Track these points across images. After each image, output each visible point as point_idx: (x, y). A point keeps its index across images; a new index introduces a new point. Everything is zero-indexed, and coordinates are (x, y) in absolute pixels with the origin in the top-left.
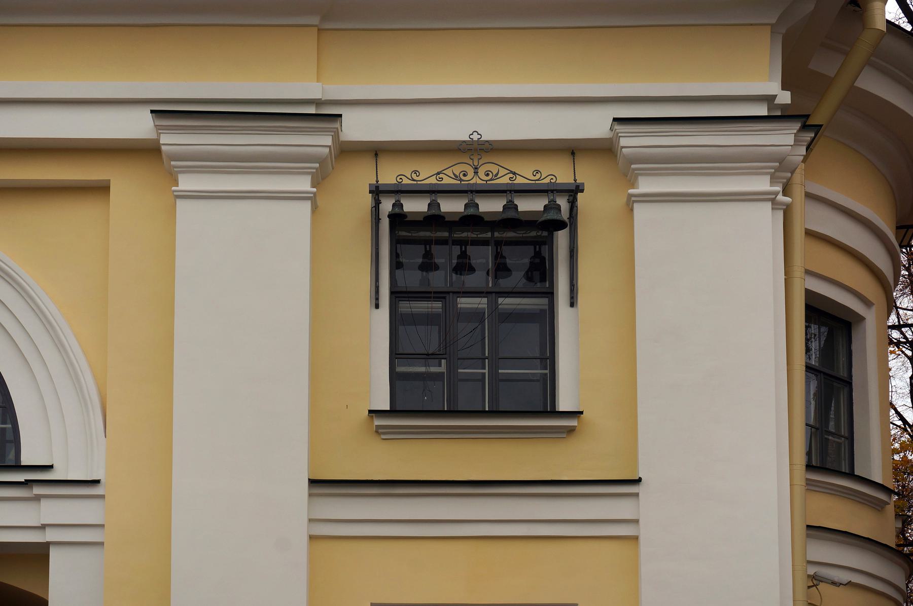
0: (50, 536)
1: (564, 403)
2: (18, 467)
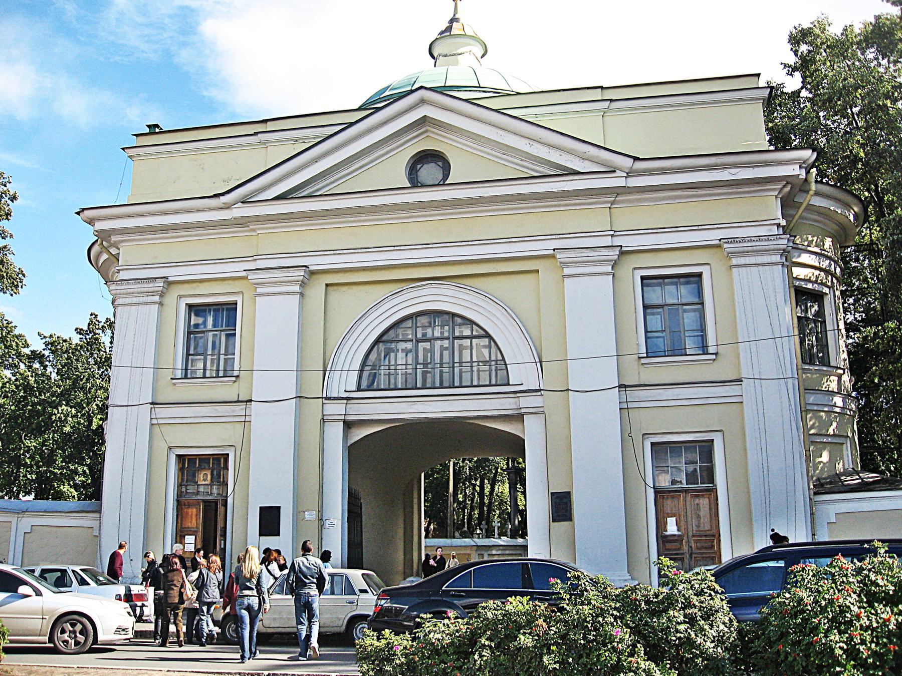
0: (523, 411)
2: (508, 384)
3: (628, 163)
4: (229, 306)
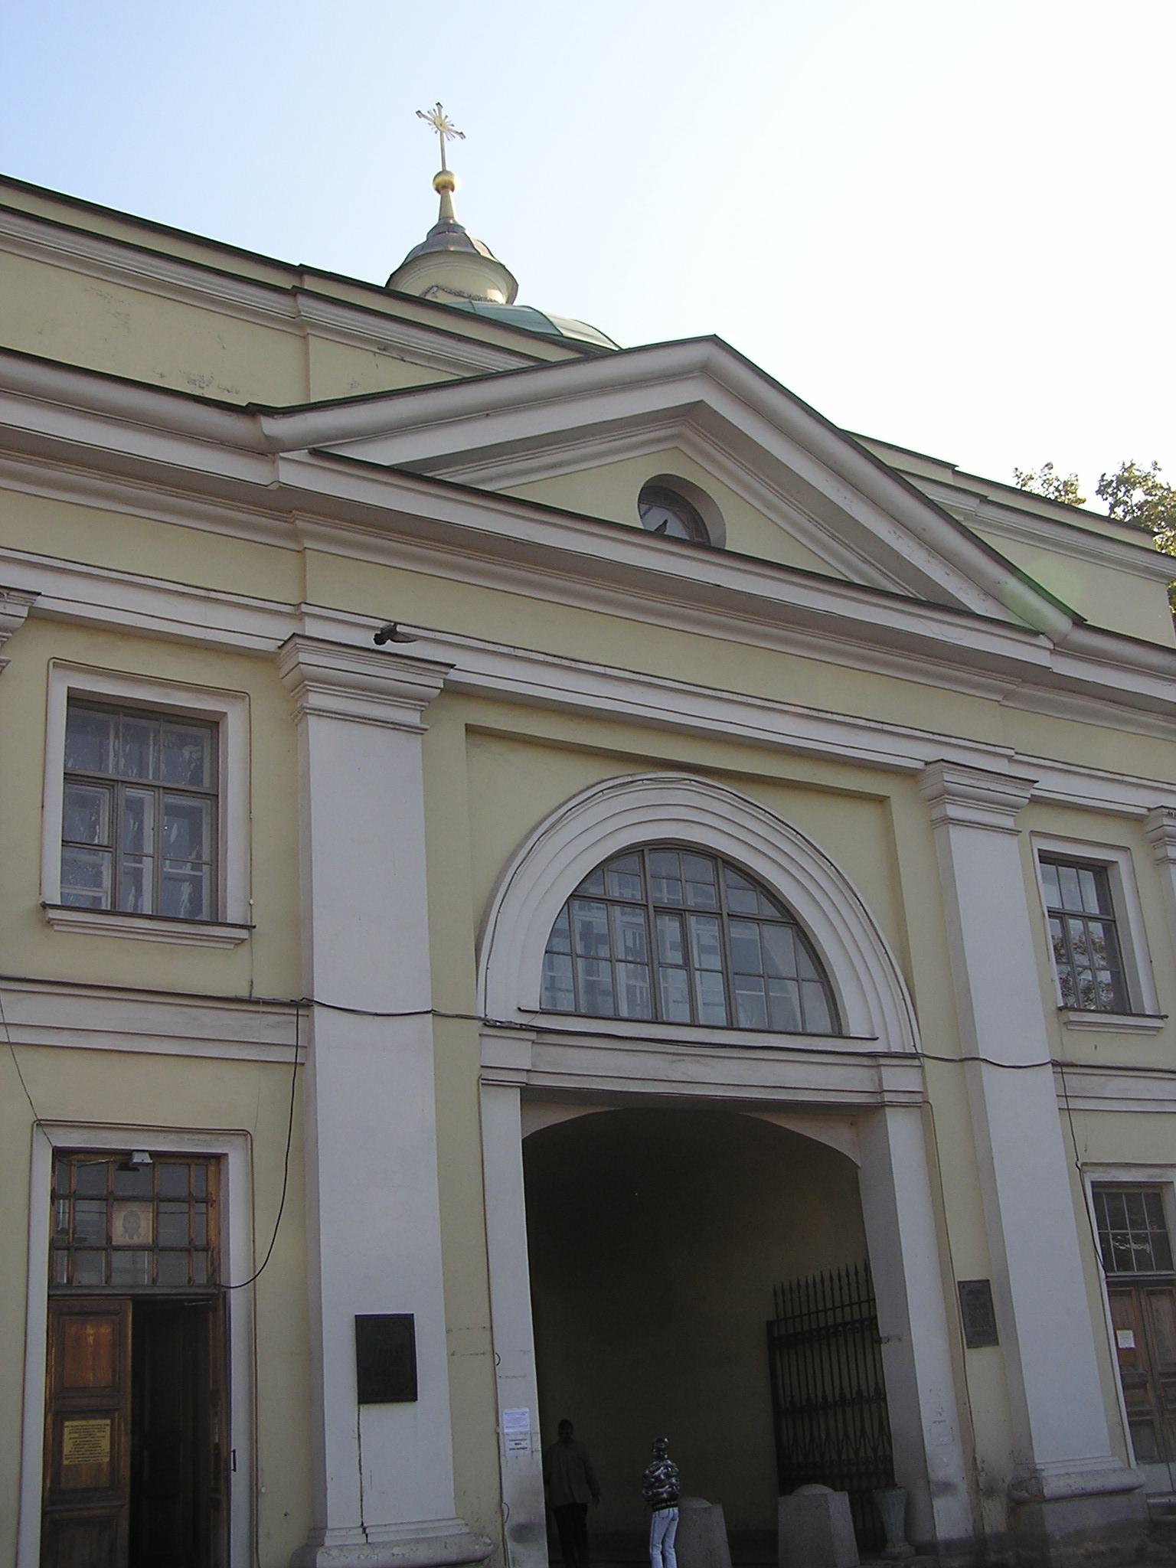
1: (234, 912)
3: (1062, 623)
4: (1122, 972)
